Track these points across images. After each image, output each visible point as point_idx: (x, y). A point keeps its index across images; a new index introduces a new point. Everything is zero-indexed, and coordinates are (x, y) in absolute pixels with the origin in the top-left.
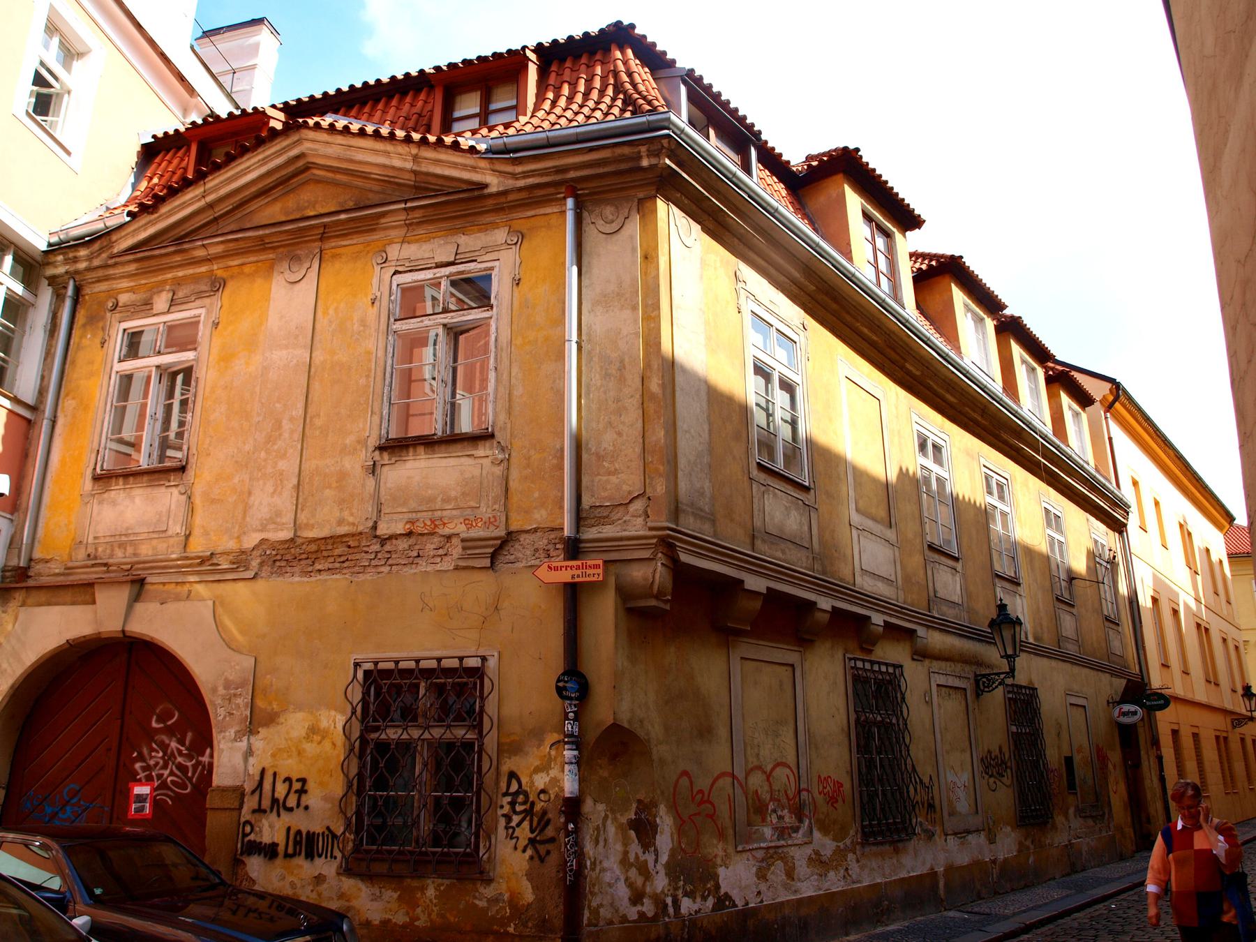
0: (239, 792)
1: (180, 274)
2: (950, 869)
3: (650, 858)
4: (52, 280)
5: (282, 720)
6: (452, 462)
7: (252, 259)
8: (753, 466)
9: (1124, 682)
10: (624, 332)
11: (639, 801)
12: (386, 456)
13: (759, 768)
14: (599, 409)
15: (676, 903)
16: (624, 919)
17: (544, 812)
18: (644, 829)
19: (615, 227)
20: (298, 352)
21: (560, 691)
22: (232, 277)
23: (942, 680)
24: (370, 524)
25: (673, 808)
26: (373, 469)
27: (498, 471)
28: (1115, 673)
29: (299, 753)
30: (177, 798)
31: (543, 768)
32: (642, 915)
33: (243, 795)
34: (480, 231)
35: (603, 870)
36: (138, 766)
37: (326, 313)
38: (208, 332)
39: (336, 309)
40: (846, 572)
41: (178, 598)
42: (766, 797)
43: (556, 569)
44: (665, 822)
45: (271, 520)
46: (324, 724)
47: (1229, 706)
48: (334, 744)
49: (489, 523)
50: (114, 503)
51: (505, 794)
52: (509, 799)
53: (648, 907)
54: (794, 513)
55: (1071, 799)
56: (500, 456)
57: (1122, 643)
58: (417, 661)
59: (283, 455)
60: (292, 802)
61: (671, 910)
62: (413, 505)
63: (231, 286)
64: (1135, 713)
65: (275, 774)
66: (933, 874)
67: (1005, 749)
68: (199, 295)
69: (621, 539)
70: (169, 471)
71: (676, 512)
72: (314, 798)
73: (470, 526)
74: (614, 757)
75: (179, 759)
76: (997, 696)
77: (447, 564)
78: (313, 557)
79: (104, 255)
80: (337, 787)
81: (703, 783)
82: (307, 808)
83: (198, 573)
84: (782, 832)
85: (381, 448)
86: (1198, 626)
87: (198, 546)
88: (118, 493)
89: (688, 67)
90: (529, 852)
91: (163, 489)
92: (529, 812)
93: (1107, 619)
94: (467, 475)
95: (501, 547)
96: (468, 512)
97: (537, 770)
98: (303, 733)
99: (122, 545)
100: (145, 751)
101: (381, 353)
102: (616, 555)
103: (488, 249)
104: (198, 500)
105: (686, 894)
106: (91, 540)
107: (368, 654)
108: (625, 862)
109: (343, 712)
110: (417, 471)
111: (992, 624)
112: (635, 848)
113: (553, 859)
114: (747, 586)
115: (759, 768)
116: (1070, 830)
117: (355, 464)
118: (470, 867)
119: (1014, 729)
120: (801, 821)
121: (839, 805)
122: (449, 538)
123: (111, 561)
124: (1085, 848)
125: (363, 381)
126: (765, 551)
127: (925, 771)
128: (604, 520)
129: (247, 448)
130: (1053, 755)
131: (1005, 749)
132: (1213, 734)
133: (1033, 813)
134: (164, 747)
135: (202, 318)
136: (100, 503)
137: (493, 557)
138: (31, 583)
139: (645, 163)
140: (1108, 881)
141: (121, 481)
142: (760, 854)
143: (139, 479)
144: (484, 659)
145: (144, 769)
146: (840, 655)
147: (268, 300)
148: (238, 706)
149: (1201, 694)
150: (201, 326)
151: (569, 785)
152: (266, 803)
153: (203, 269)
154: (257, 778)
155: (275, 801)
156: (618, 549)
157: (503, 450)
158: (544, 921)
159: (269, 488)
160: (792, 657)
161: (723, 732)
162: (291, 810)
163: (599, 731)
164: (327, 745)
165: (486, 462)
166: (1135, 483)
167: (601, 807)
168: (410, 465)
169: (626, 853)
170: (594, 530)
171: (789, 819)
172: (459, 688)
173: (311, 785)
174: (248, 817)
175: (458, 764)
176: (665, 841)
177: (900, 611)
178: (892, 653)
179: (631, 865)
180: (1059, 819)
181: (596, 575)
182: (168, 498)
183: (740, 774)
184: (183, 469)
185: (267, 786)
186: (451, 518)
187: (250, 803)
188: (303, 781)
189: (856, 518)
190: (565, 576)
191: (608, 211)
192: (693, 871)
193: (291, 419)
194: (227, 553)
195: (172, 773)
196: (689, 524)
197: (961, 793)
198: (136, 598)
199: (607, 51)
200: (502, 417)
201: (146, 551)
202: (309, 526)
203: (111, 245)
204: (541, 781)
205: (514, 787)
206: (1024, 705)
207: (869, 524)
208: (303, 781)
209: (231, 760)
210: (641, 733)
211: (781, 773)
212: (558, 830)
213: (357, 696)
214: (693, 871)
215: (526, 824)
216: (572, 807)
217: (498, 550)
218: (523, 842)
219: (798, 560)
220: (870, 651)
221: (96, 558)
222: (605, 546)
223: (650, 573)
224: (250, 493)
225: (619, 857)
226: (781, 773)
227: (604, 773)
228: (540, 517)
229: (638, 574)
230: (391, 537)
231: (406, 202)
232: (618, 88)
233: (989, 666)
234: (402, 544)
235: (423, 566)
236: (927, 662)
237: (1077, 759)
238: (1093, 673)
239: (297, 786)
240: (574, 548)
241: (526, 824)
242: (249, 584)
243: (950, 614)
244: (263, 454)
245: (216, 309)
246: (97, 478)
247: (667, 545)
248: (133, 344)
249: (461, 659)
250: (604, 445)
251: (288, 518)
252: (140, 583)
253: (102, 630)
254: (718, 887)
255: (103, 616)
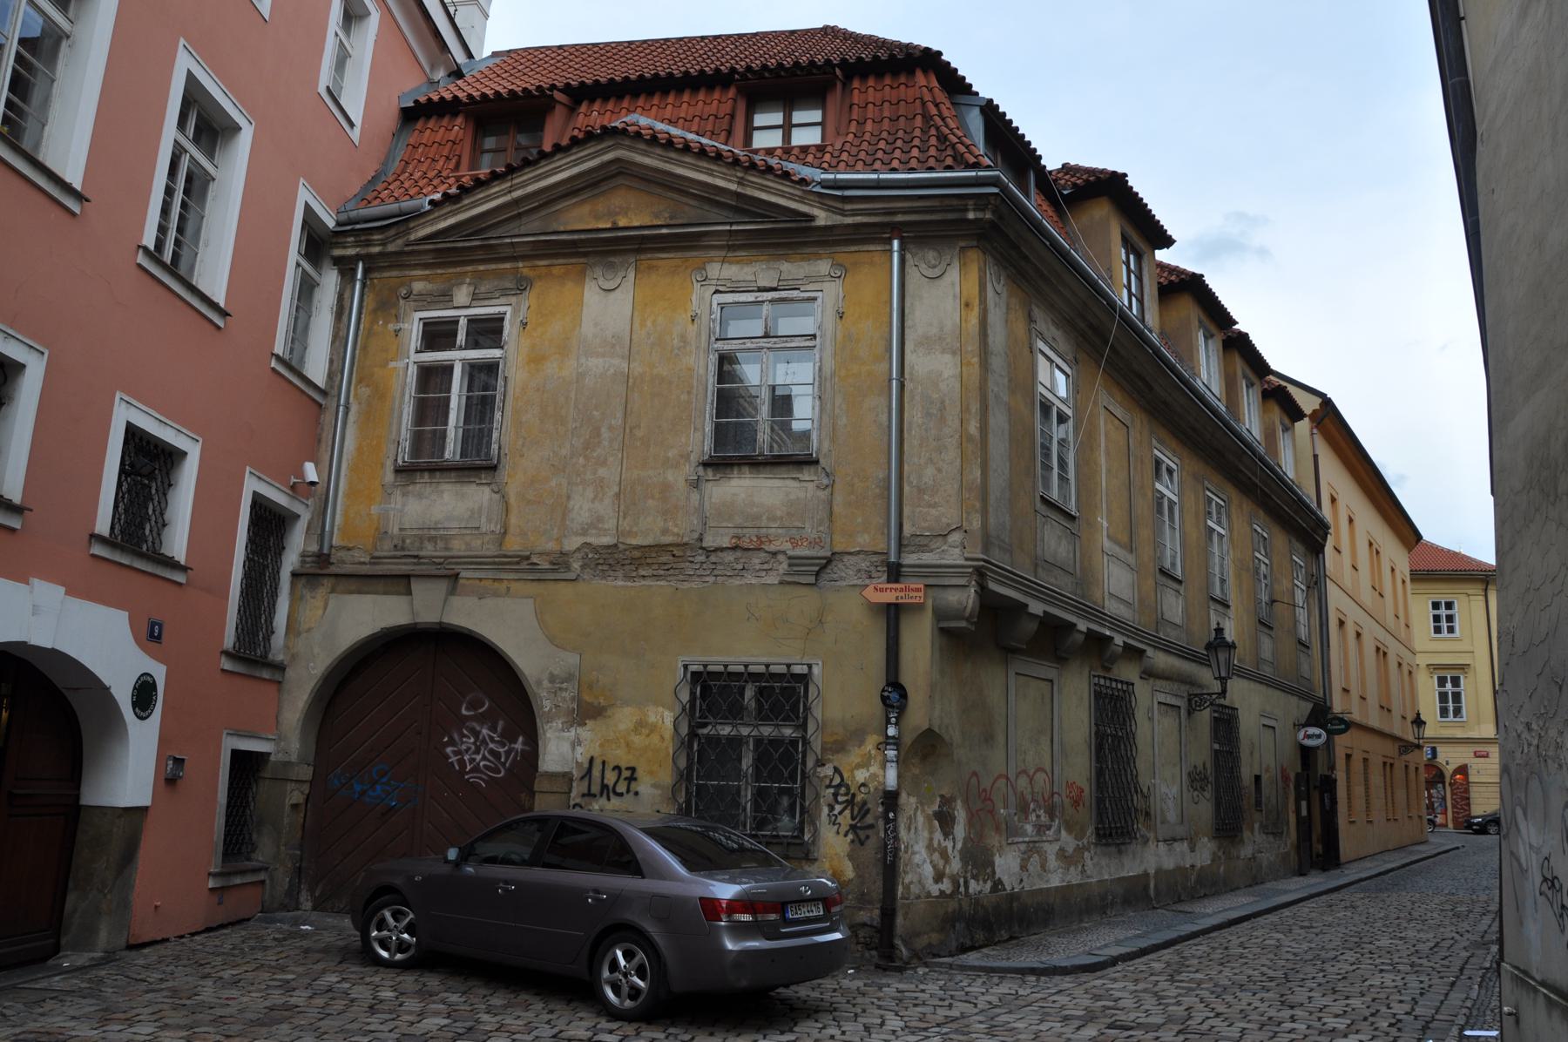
0: (567, 777)
1: (481, 268)
2: (1159, 871)
3: (949, 844)
4: (338, 262)
5: (609, 713)
6: (777, 483)
7: (561, 261)
8: (1038, 499)
9: (1310, 706)
10: (946, 375)
11: (942, 796)
12: (710, 472)
13: (1025, 772)
14: (921, 445)
15: (966, 883)
16: (929, 895)
17: (864, 803)
18: (945, 820)
19: (937, 272)
20: (616, 361)
21: (884, 699)
22: (540, 277)
23: (1162, 698)
24: (696, 535)
25: (966, 802)
26: (696, 484)
27: (823, 495)
28: (1304, 696)
29: (628, 745)
30: (492, 781)
31: (865, 765)
32: (942, 892)
33: (571, 780)
34: (803, 260)
35: (914, 853)
36: (449, 750)
37: (643, 324)
38: (515, 332)
39: (654, 322)
40: (1097, 595)
41: (496, 594)
42: (1029, 798)
43: (881, 590)
44: (961, 814)
45: (592, 525)
46: (652, 719)
47: (1397, 732)
48: (662, 738)
49: (813, 544)
50: (420, 496)
51: (829, 786)
52: (832, 790)
53: (946, 886)
54: (1064, 542)
55: (1257, 816)
56: (825, 481)
57: (1310, 667)
58: (746, 666)
59: (603, 463)
60: (621, 788)
61: (962, 889)
62: (738, 520)
63: (538, 286)
64: (1319, 736)
65: (604, 763)
66: (1146, 874)
67: (1208, 766)
68: (505, 292)
69: (940, 566)
70: (478, 465)
71: (986, 547)
72: (644, 787)
73: (795, 545)
74: (924, 758)
75: (491, 746)
76: (1205, 716)
77: (772, 579)
78: (637, 563)
79: (400, 242)
80: (667, 776)
81: (986, 783)
82: (636, 793)
83: (516, 571)
84: (1041, 829)
85: (705, 465)
86: (1378, 649)
87: (513, 545)
88: (422, 484)
89: (988, 97)
90: (850, 836)
91: (473, 487)
92: (850, 803)
93: (1300, 642)
94: (792, 497)
95: (824, 567)
96: (794, 531)
97: (858, 766)
98: (631, 726)
99: (432, 539)
100: (456, 737)
101: (702, 371)
102: (934, 576)
103: (810, 279)
104: (512, 500)
105: (975, 877)
106: (396, 531)
107: (698, 658)
108: (930, 847)
109: (671, 709)
110: (741, 488)
111: (1209, 646)
112: (938, 835)
113: (872, 843)
114: (1031, 610)
115: (1025, 772)
116: (1255, 844)
117: (678, 478)
118: (800, 851)
119: (1216, 746)
120: (1052, 820)
121: (1080, 808)
122: (774, 554)
123: (422, 553)
124: (1265, 863)
125: (684, 397)
126: (1048, 580)
127: (1144, 781)
128: (923, 548)
129: (564, 452)
130: (1246, 773)
131: (1208, 766)
132: (1381, 760)
133: (1227, 829)
134: (476, 734)
135: (508, 317)
136: (404, 495)
137: (818, 574)
138: (333, 569)
139: (971, 215)
140: (1286, 892)
141: (426, 475)
142: (1023, 847)
143: (446, 474)
144: (810, 666)
145: (456, 753)
146: (1086, 672)
147: (581, 304)
148: (564, 699)
149: (1374, 721)
150: (507, 324)
151: (891, 778)
152: (595, 789)
153: (508, 266)
154: (586, 765)
155: (604, 787)
156: (937, 575)
157: (827, 475)
158: (863, 894)
159: (590, 493)
160: (1051, 673)
161: (1001, 739)
162: (621, 795)
163: (915, 735)
164: (655, 739)
165: (811, 486)
166: (1333, 500)
167: (913, 800)
168: (735, 482)
169: (931, 839)
170: (914, 556)
171: (1044, 818)
172: (785, 694)
173: (640, 773)
174: (578, 801)
175: (783, 762)
176: (960, 830)
177: (1136, 632)
178: (1128, 672)
179: (935, 850)
180: (1246, 834)
181: (917, 597)
182: (478, 496)
183: (1012, 777)
184: (494, 468)
185: (596, 773)
186: (777, 536)
187: (578, 789)
188: (633, 769)
189: (1107, 544)
190: (890, 597)
191: (931, 255)
192: (978, 859)
193: (611, 428)
194: (548, 554)
195: (484, 758)
196: (997, 557)
197: (1170, 803)
198: (452, 591)
199: (911, 73)
200: (826, 445)
201: (458, 547)
202: (630, 533)
203: (408, 231)
204: (861, 776)
205: (837, 780)
206: (1226, 724)
207: (1117, 549)
208: (633, 769)
209: (560, 749)
210: (946, 738)
211: (1040, 777)
212: (877, 818)
213: (685, 697)
214: (978, 859)
215: (847, 812)
216: (891, 800)
217: (818, 569)
218: (844, 828)
219: (1064, 585)
220: (1108, 670)
221: (403, 549)
222: (923, 571)
223: (965, 598)
224: (569, 497)
225: (926, 843)
226: (1040, 777)
227: (917, 771)
228: (864, 540)
229: (953, 598)
230: (716, 550)
231: (731, 224)
232: (942, 138)
233: (1201, 686)
234: (729, 557)
235: (750, 579)
236: (1151, 681)
237: (1264, 778)
238: (1282, 695)
239: (626, 774)
240: (895, 573)
241: (847, 812)
242: (570, 585)
243: (1172, 635)
244: (581, 460)
245: (524, 308)
246: (398, 471)
247: (980, 574)
248: (438, 335)
249: (789, 666)
250: (925, 479)
251: (610, 524)
252: (456, 577)
253: (419, 620)
254: (994, 872)
255: (425, 606)
